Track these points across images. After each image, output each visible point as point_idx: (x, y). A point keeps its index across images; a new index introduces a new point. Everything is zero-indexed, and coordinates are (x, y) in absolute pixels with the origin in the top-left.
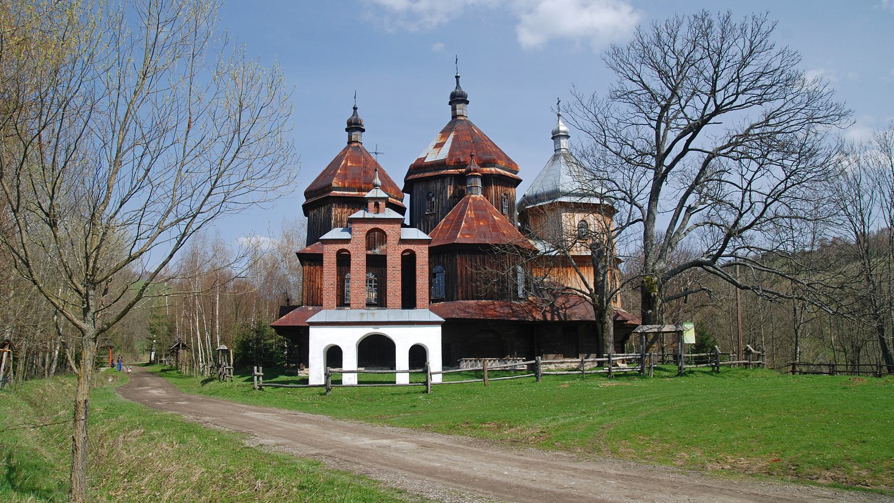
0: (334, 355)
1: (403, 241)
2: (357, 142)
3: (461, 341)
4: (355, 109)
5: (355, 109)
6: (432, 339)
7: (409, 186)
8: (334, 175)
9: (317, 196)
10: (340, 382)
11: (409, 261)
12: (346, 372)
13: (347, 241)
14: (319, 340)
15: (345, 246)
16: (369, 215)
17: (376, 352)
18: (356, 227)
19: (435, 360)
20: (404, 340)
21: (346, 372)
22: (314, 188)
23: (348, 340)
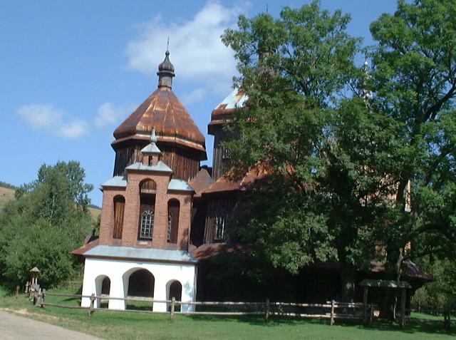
0: (105, 285)
1: (170, 192)
2: (166, 86)
3: (214, 284)
4: (167, 54)
5: (167, 54)
6: (187, 276)
7: (212, 129)
8: (139, 120)
9: (123, 137)
10: (151, 308)
11: (173, 204)
12: (156, 302)
13: (123, 189)
14: (93, 270)
15: (121, 193)
16: (144, 167)
17: (140, 283)
18: (131, 177)
19: (187, 297)
20: (163, 276)
21: (156, 302)
22: (122, 131)
23: (118, 272)
